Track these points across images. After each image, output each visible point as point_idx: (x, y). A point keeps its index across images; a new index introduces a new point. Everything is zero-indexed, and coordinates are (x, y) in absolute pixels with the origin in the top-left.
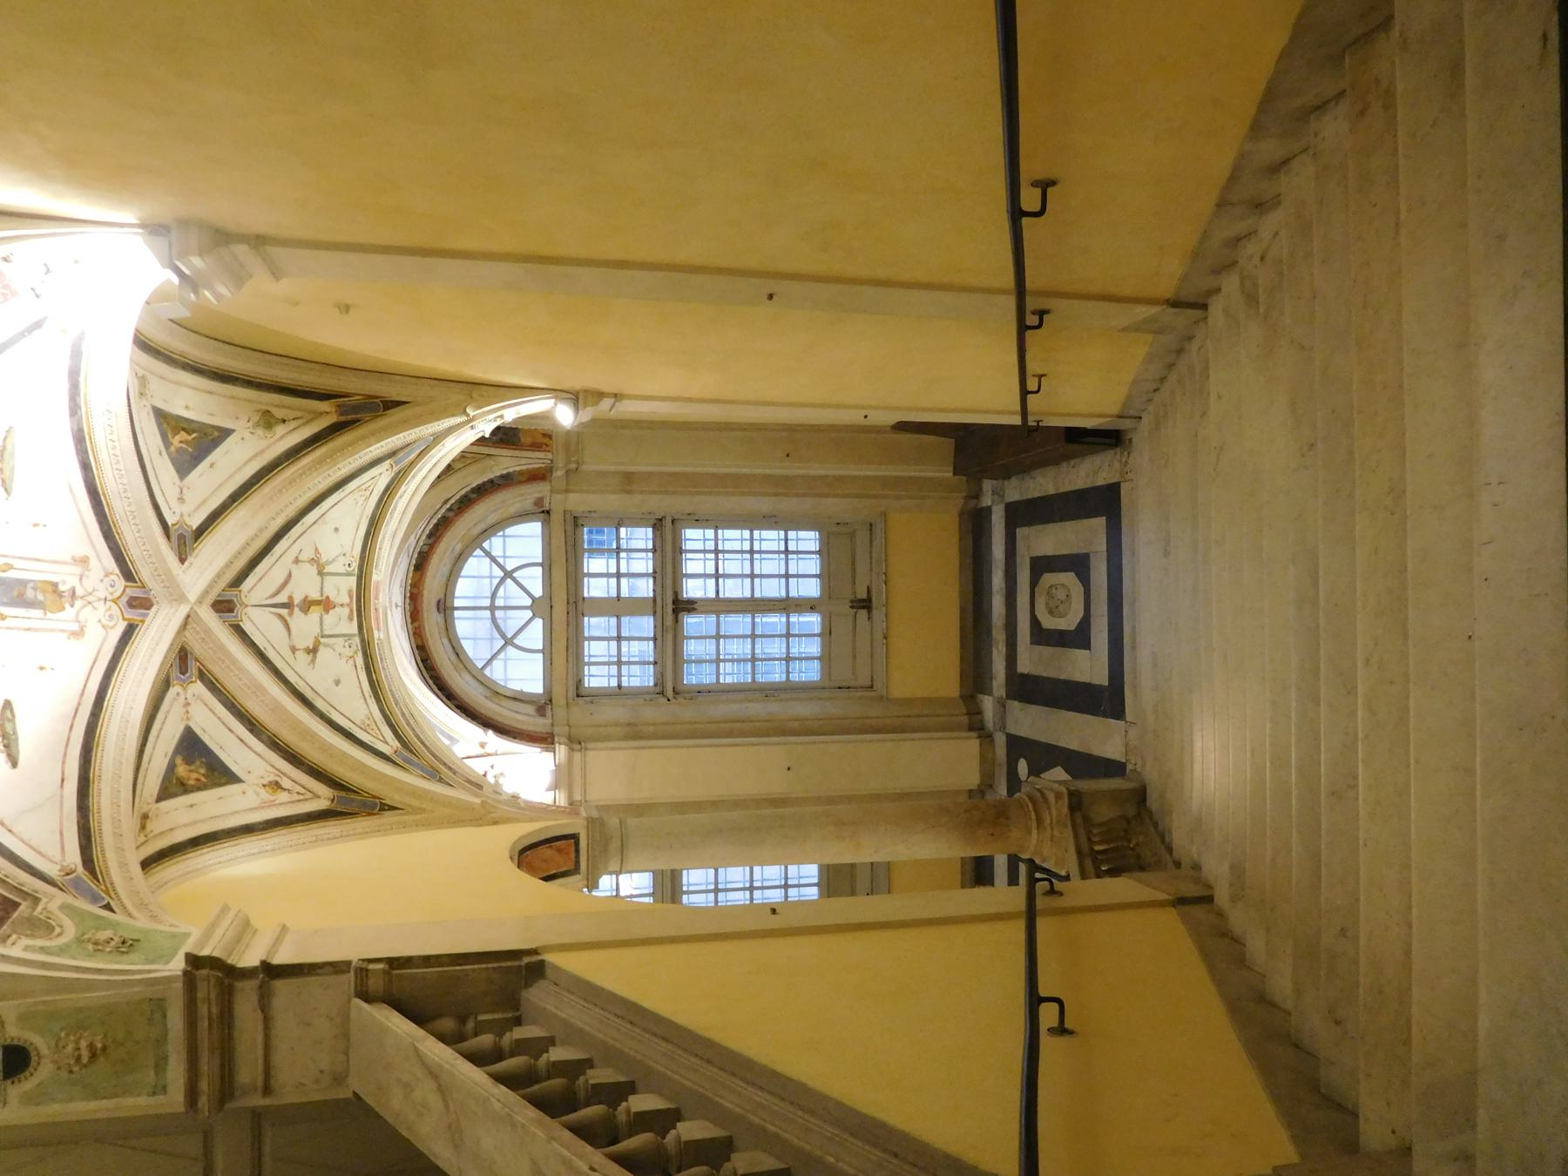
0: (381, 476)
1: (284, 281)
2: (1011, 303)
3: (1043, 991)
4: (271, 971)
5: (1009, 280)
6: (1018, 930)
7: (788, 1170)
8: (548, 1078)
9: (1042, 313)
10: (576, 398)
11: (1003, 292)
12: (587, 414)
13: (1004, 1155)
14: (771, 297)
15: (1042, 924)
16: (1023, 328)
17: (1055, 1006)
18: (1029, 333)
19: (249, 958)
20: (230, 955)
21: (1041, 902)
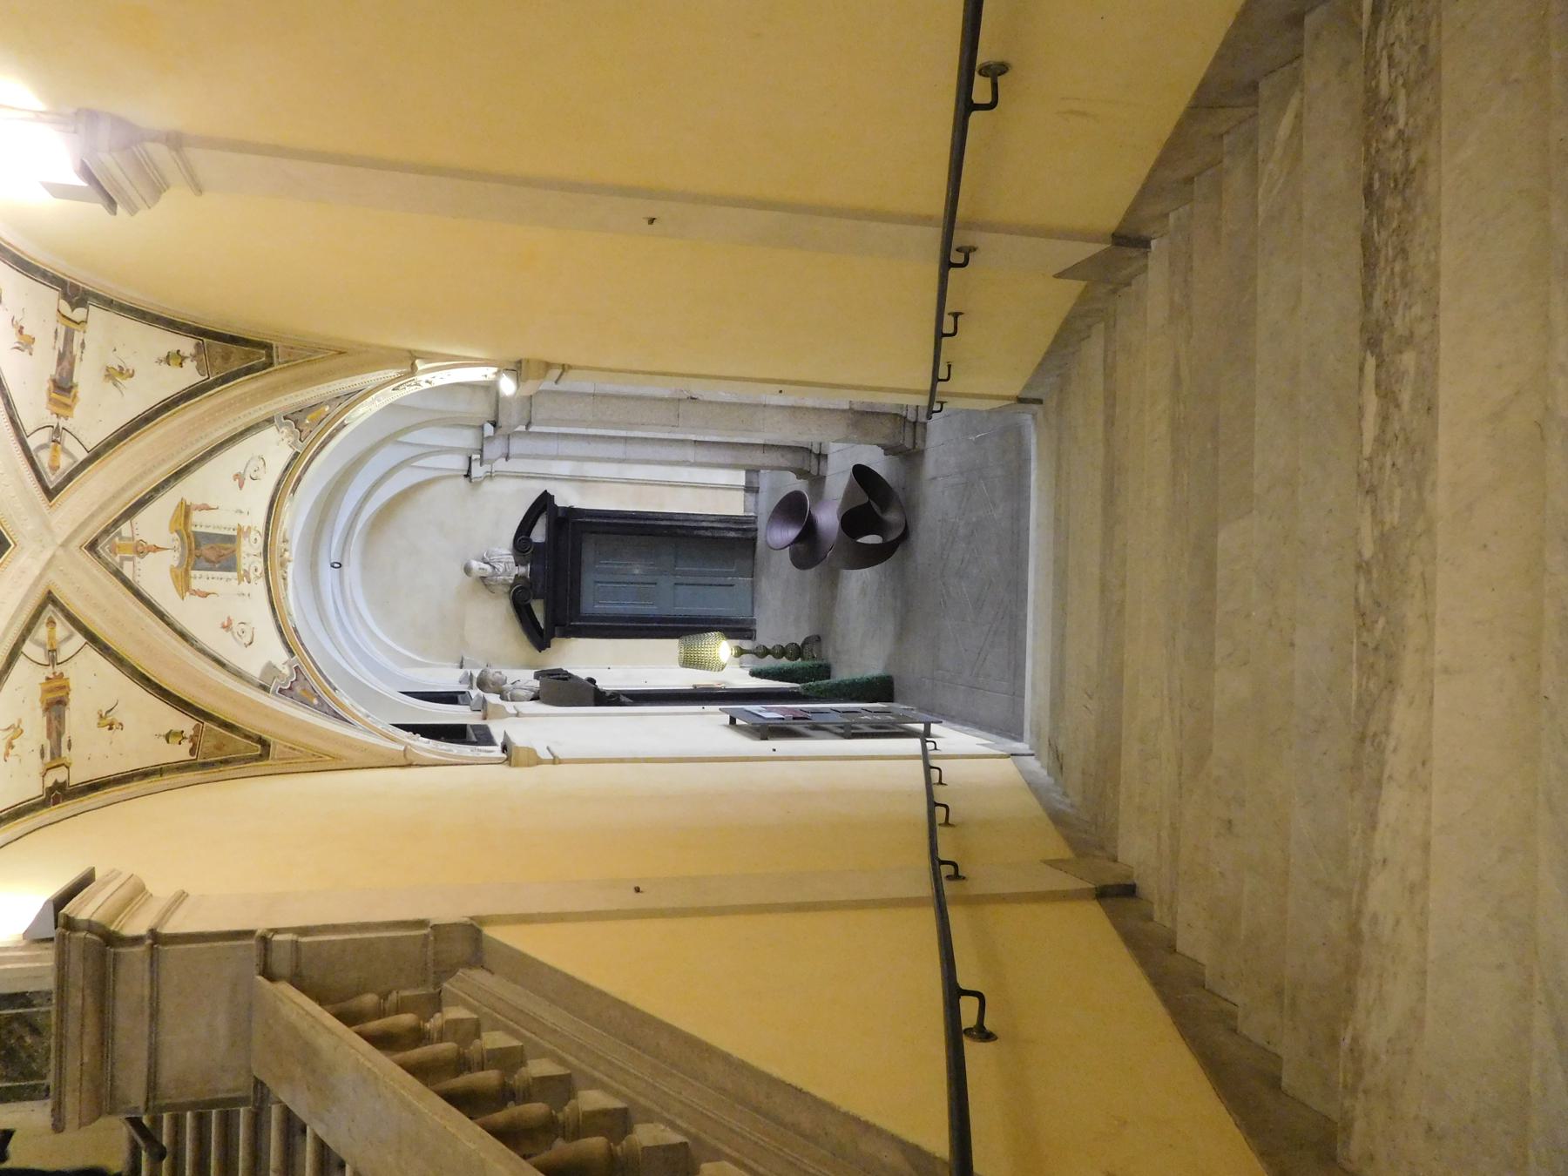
0: (274, 447)
1: (139, 214)
2: (934, 234)
3: (964, 984)
4: (156, 938)
5: (938, 207)
6: (927, 919)
7: (569, 1076)
8: (441, 1040)
9: (968, 252)
10: (518, 369)
11: (926, 220)
12: (530, 387)
13: (938, 1143)
14: (652, 221)
15: (955, 915)
16: (947, 265)
17: (975, 1001)
18: (953, 272)
19: (136, 926)
20: (112, 922)
21: (949, 888)
